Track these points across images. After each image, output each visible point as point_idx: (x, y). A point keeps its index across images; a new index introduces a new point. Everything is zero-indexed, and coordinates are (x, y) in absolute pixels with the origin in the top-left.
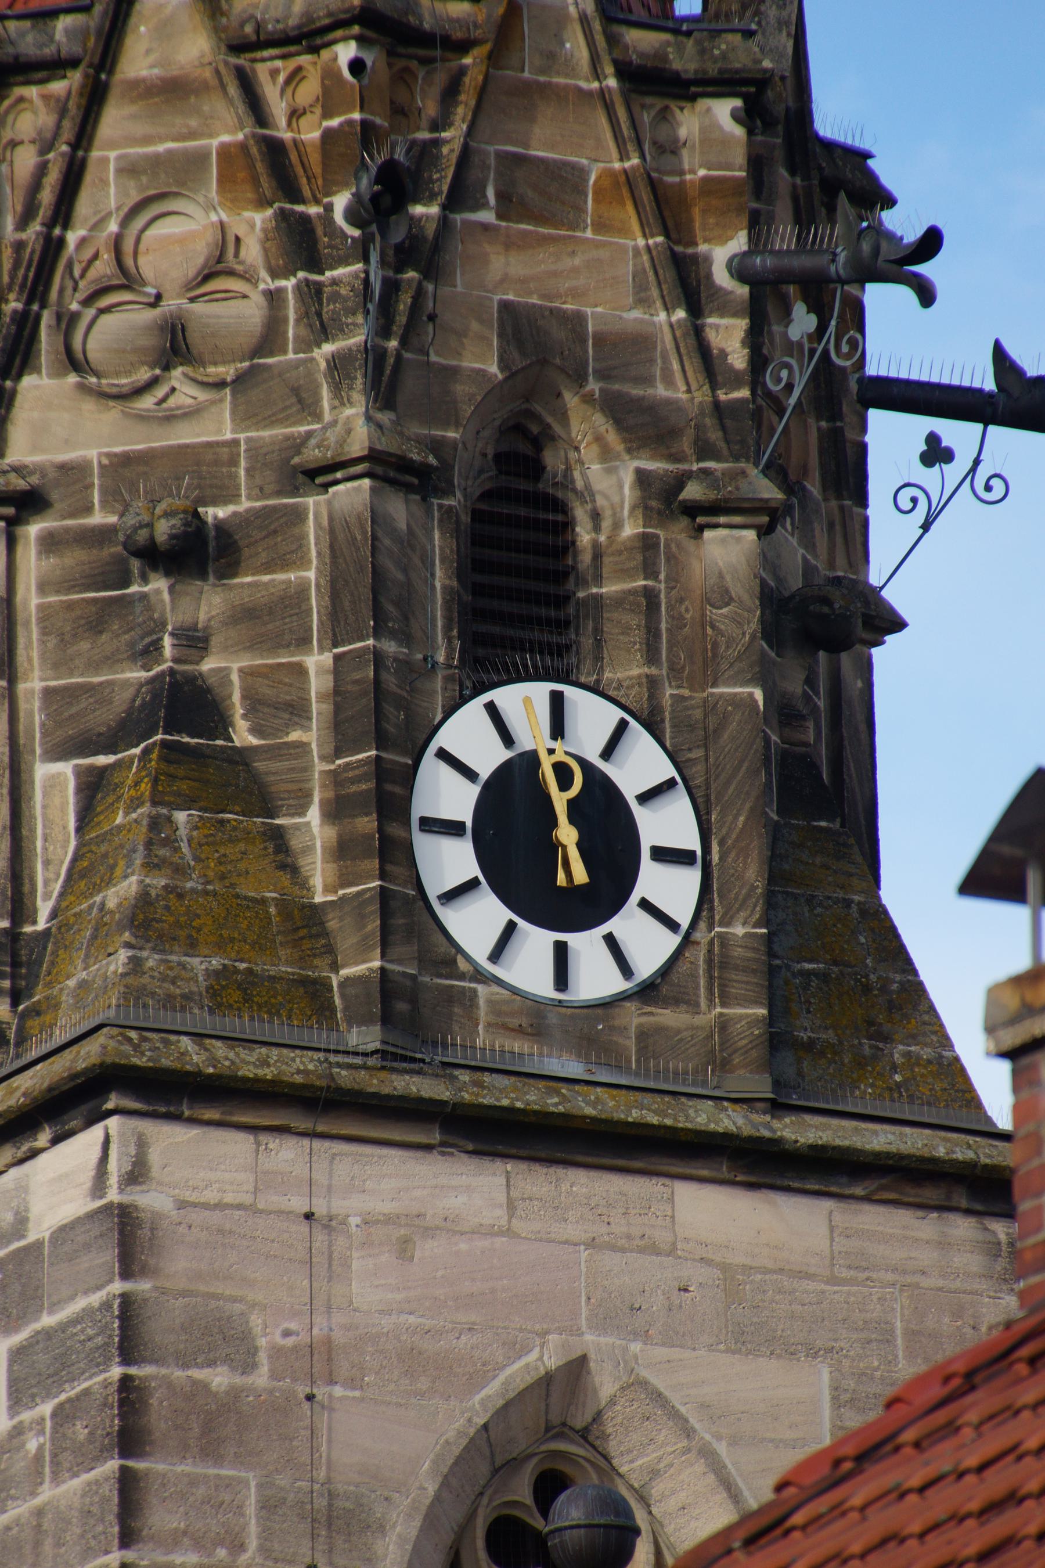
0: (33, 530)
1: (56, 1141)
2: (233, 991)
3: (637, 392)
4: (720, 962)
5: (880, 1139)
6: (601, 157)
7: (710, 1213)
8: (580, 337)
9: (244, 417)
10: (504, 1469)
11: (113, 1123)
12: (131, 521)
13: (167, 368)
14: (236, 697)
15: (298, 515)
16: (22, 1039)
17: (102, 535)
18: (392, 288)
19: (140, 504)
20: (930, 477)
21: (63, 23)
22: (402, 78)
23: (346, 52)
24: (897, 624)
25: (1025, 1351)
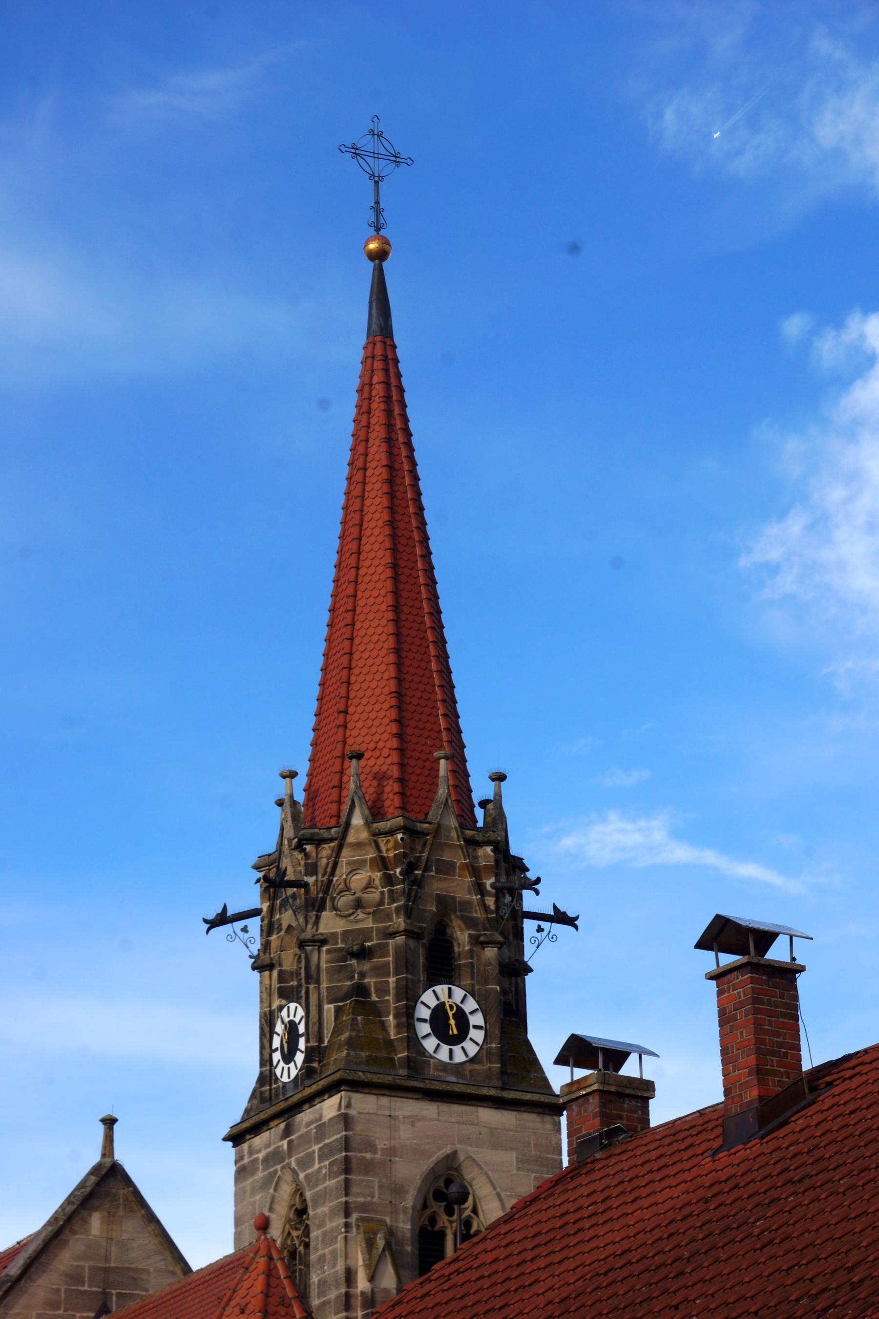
0: (325, 948)
1: (329, 1097)
2: (371, 1061)
3: (469, 915)
4: (489, 1052)
5: (528, 1097)
6: (460, 860)
7: (487, 1115)
8: (455, 902)
9: (375, 921)
10: (437, 1178)
11: (343, 1093)
12: (348, 946)
13: (357, 909)
14: (373, 989)
15: (388, 944)
16: (321, 1072)
17: (341, 949)
18: (410, 890)
19: (350, 942)
20: (538, 935)
21: (333, 830)
22: (413, 841)
23: (400, 836)
24: (531, 970)
25: (569, 1176)
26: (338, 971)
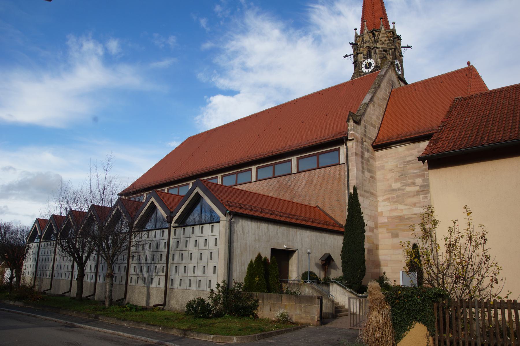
26: (380, 54)
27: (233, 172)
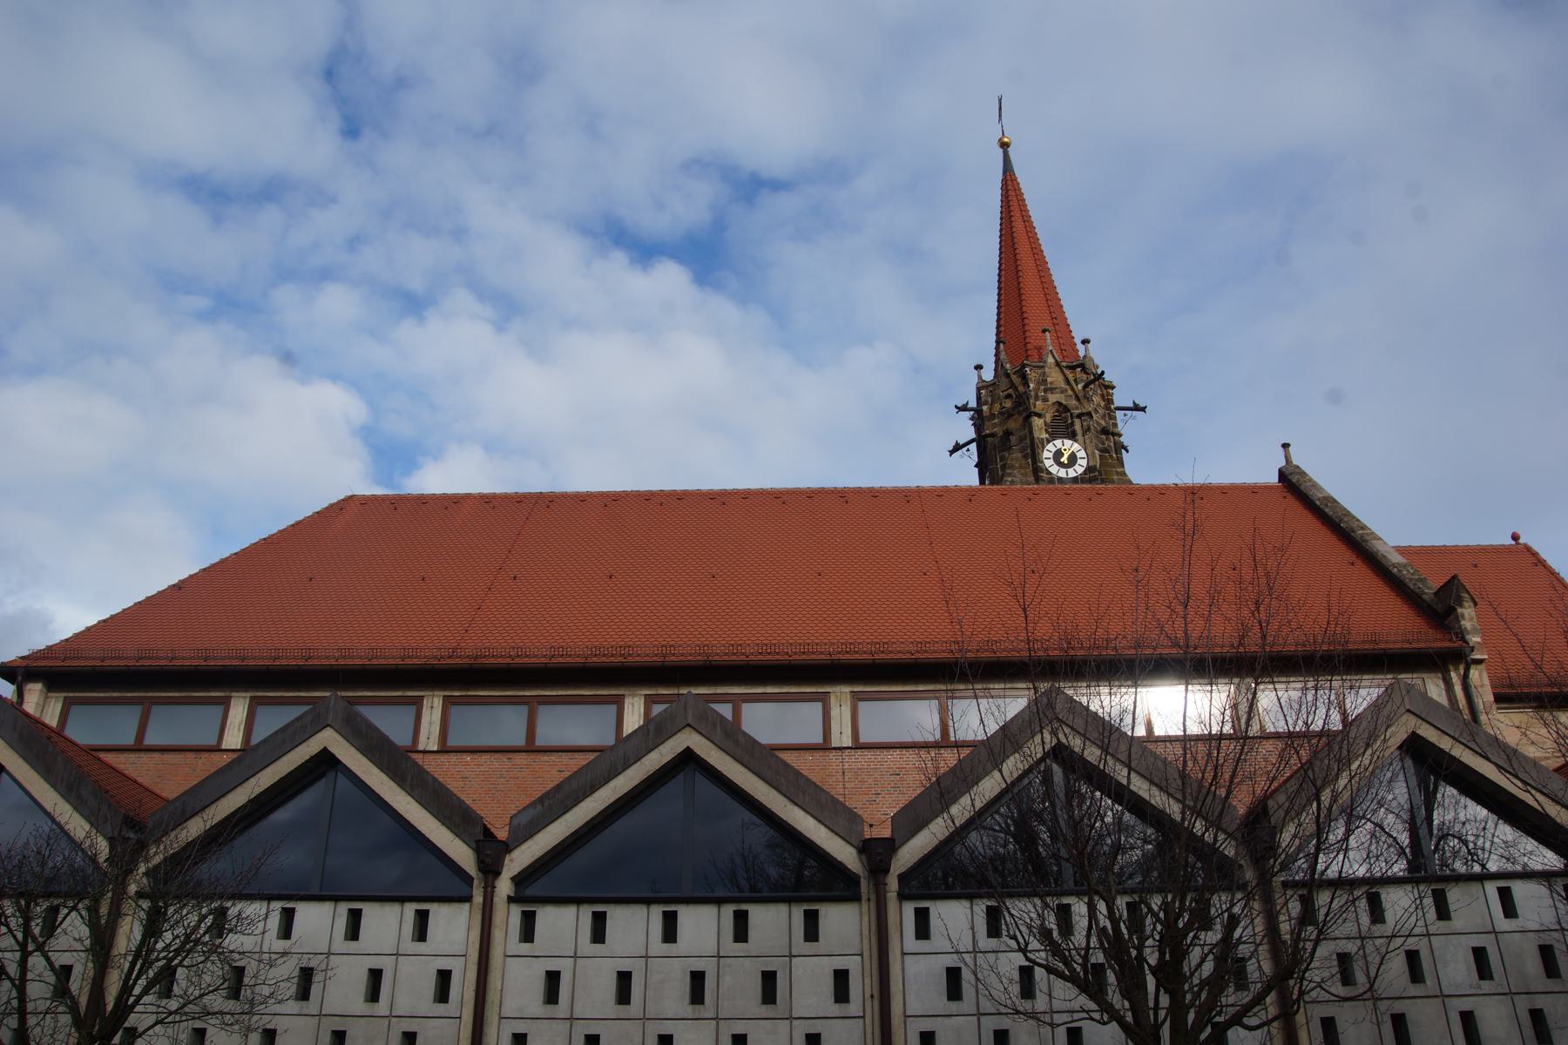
27: (785, 690)
